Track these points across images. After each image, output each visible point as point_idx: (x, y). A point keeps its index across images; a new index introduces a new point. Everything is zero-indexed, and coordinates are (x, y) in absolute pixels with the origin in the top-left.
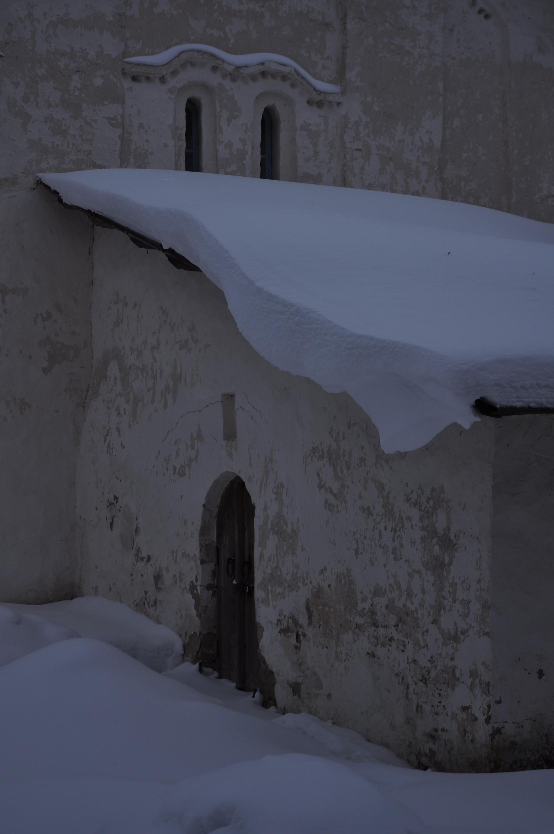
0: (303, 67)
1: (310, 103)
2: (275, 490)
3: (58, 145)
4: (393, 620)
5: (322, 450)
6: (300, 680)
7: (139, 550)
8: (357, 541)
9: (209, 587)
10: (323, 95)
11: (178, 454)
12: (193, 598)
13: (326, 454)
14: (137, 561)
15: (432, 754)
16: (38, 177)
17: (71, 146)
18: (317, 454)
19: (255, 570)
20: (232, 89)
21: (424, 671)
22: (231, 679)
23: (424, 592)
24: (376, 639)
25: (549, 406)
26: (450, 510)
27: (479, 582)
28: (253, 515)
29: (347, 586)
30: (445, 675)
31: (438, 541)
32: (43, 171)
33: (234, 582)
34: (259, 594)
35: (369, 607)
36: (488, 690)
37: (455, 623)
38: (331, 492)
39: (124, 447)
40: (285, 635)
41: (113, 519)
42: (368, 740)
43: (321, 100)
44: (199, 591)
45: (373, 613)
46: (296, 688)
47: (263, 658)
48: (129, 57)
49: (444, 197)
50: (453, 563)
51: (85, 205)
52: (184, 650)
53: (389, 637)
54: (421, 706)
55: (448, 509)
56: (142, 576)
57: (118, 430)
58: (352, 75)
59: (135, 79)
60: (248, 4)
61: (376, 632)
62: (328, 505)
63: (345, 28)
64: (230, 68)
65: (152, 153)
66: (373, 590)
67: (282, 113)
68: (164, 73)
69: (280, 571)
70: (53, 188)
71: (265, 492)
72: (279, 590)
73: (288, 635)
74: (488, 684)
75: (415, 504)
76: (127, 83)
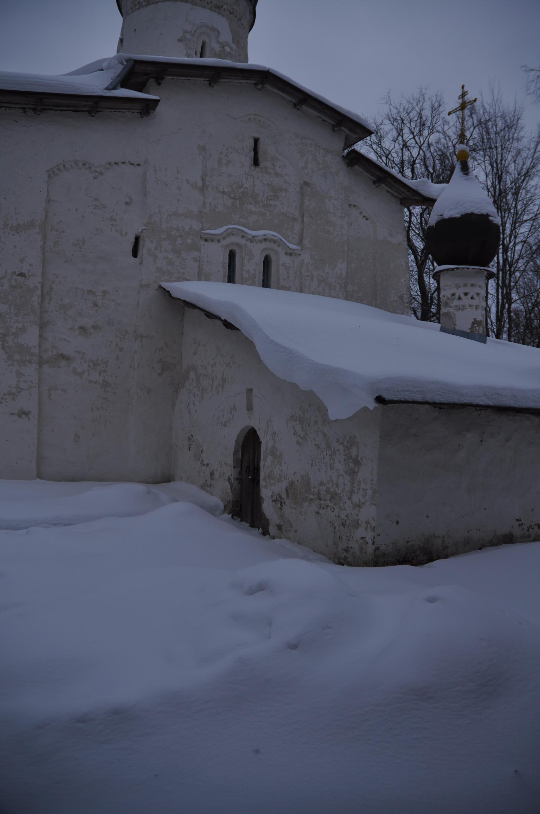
1: (286, 254)
2: (272, 435)
3: (169, 270)
4: (329, 497)
5: (296, 417)
6: (282, 524)
7: (203, 461)
8: (312, 460)
9: (237, 479)
11: (223, 416)
12: (229, 484)
14: (202, 466)
15: (346, 558)
16: (160, 284)
17: (175, 270)
18: (293, 418)
22: (246, 522)
23: (344, 484)
25: (409, 400)
27: (372, 480)
28: (260, 446)
30: (353, 523)
31: (352, 461)
32: (162, 281)
33: (250, 477)
34: (262, 483)
35: (317, 491)
36: (374, 530)
37: (359, 499)
38: (300, 437)
39: (196, 412)
40: (275, 503)
41: (190, 446)
42: (315, 552)
43: (291, 253)
44: (232, 481)
45: (319, 494)
46: (279, 527)
47: (264, 513)
48: (204, 230)
49: (347, 299)
50: (360, 472)
51: (183, 298)
52: (224, 508)
53: (327, 505)
54: (341, 537)
56: (204, 473)
57: (194, 404)
58: (305, 242)
59: (206, 240)
60: (259, 208)
61: (320, 503)
62: (298, 443)
63: (303, 221)
64: (250, 237)
65: (212, 274)
66: (319, 483)
67: (273, 257)
70: (167, 289)
71: (267, 435)
72: (273, 482)
73: (276, 502)
74: (374, 527)
75: (342, 444)
76: (202, 242)
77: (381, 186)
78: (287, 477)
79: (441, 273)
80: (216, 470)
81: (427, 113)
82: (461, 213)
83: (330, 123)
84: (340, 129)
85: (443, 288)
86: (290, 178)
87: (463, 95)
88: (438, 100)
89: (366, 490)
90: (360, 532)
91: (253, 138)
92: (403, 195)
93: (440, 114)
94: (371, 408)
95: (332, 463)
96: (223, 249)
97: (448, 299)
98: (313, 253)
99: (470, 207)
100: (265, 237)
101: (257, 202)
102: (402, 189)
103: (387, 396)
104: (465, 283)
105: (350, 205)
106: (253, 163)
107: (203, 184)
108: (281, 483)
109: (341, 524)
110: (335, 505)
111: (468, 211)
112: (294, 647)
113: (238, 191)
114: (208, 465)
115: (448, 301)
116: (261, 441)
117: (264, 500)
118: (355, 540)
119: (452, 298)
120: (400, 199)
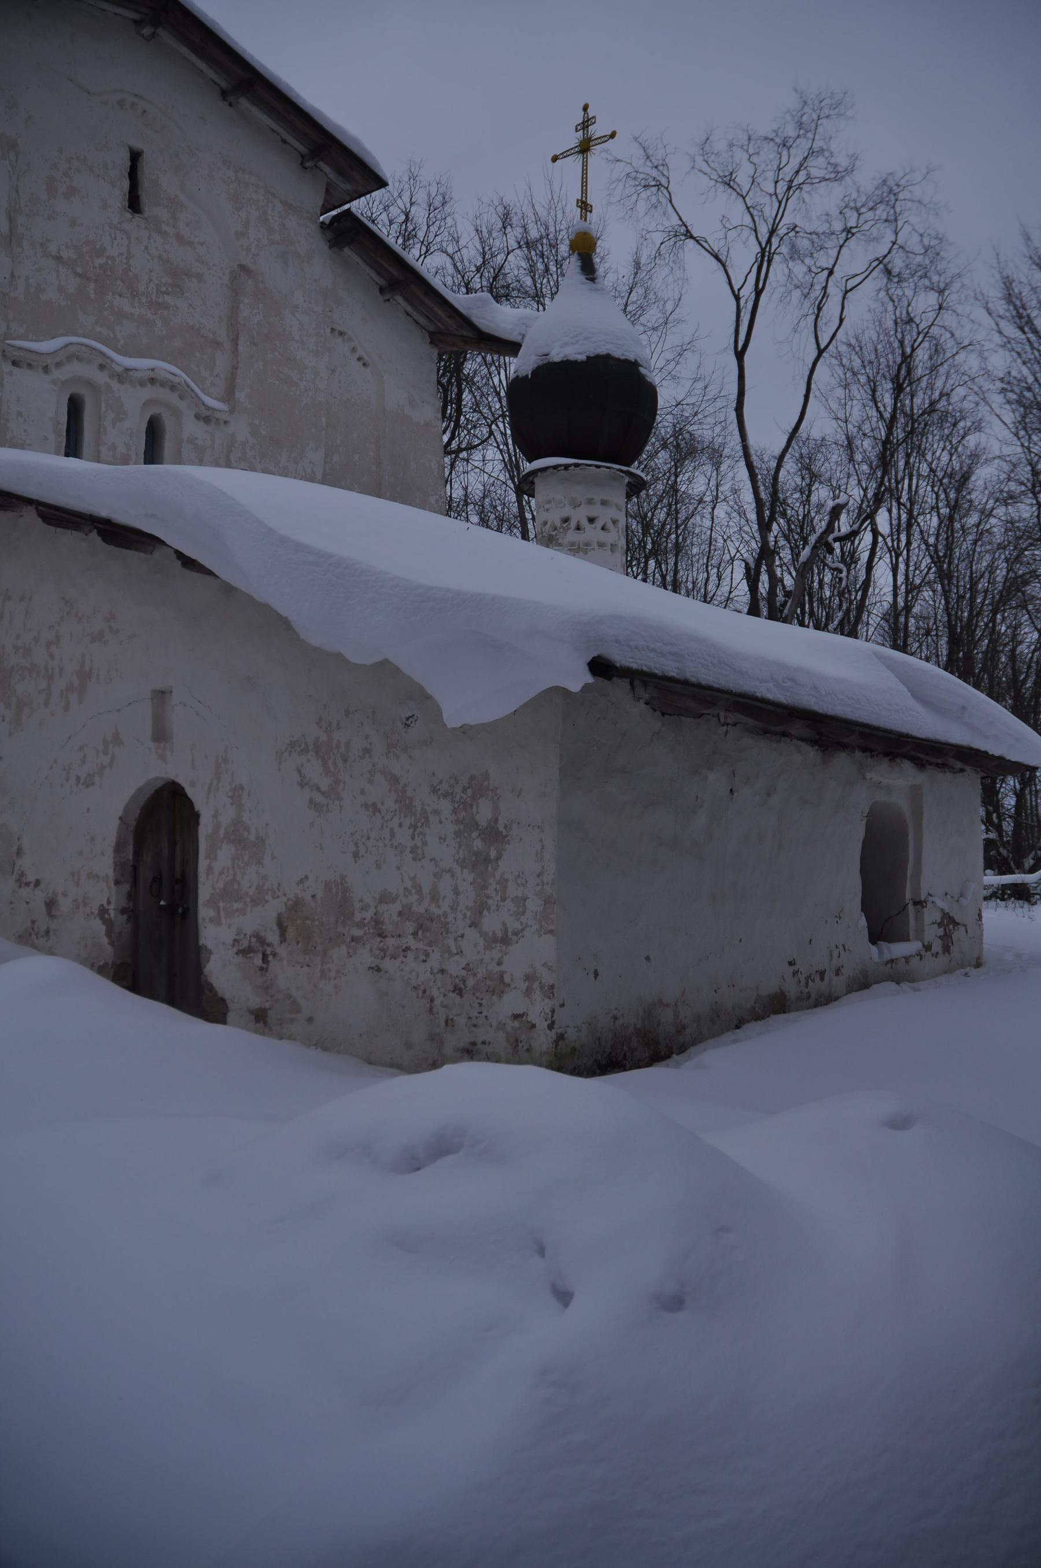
0: (192, 379)
1: (197, 417)
2: (230, 794)
4: (409, 927)
5: (306, 743)
6: (267, 1006)
7: (22, 875)
9: (123, 911)
10: (211, 410)
13: (311, 747)
14: (20, 887)
19: (200, 886)
20: (119, 390)
21: (457, 980)
23: (456, 892)
24: (382, 951)
26: (498, 799)
29: (340, 894)
30: (488, 982)
31: (480, 835)
33: (162, 903)
34: (204, 912)
35: (372, 918)
36: (552, 993)
38: (318, 789)
40: (246, 957)
47: (211, 985)
53: (404, 947)
54: (452, 1020)
55: (496, 798)
56: (27, 903)
58: (240, 395)
59: (15, 363)
60: (140, 309)
61: (382, 944)
63: (236, 349)
64: (119, 369)
66: (378, 896)
67: (169, 423)
68: (49, 362)
69: (239, 884)
74: (552, 987)
75: (446, 795)
76: (7, 367)
77: (395, 300)
78: (279, 890)
79: (537, 475)
80: (63, 894)
81: (419, 214)
82: (587, 354)
83: (296, 149)
84: (316, 166)
85: (543, 507)
86: (209, 252)
87: (586, 124)
88: (441, 191)
89: (526, 900)
90: (512, 1002)
91: (128, 149)
92: (439, 324)
93: (445, 218)
94: (575, 687)
95: (419, 844)
96: (56, 388)
97: (555, 529)
98: (257, 422)
99: (603, 343)
100: (151, 374)
101: (135, 293)
102: (437, 310)
103: (621, 658)
104: (590, 496)
105: (333, 330)
106: (127, 204)
107: (12, 230)
108: (263, 906)
109: (452, 988)
110: (430, 944)
111: (601, 350)
112: (675, 1303)
113: (93, 263)
114: (38, 883)
115: (554, 533)
116: (198, 811)
117: (210, 952)
118: (494, 1023)
119: (564, 528)
120: (429, 332)
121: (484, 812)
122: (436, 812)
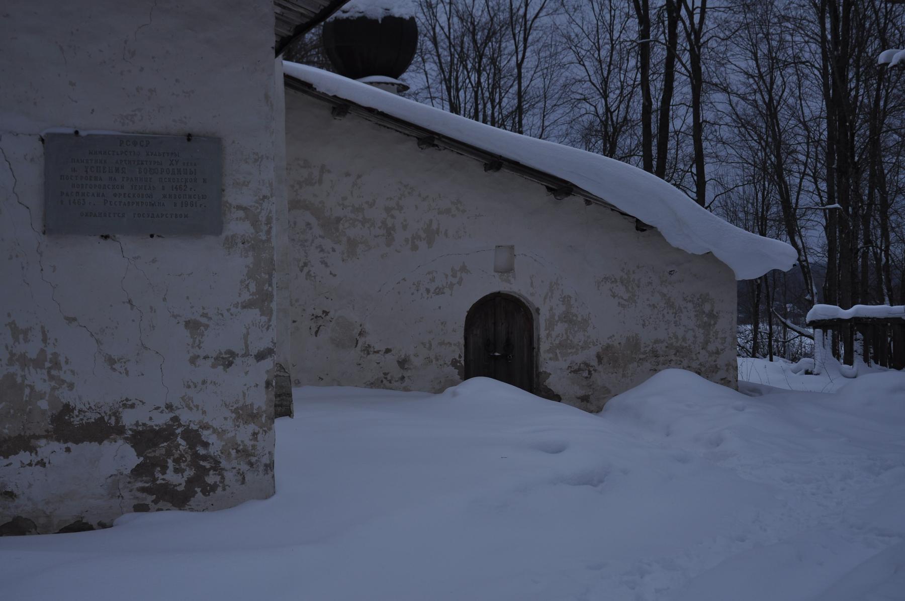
4: (673, 352)
6: (590, 393)
30: (711, 369)
35: (650, 350)
38: (622, 298)
75: (690, 301)
78: (597, 342)
110: (683, 357)
121: (707, 307)
122: (685, 308)
